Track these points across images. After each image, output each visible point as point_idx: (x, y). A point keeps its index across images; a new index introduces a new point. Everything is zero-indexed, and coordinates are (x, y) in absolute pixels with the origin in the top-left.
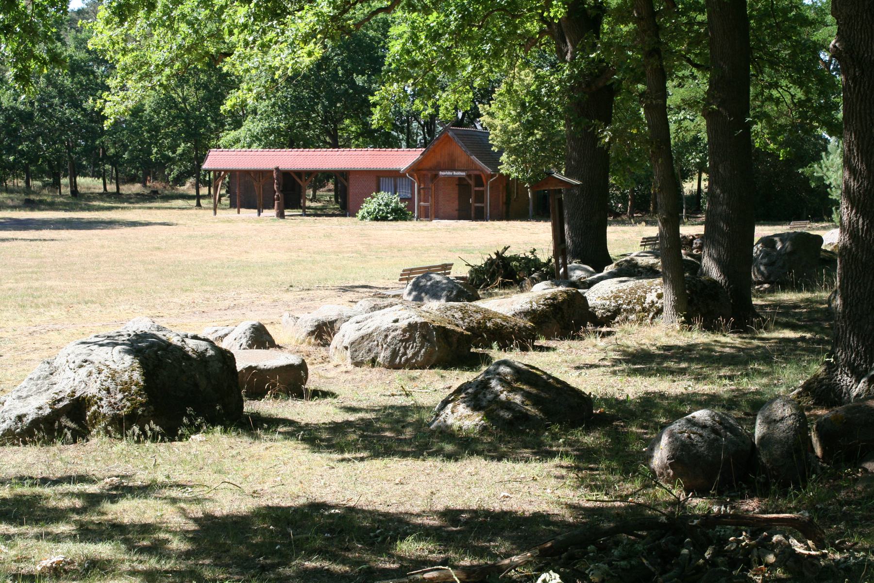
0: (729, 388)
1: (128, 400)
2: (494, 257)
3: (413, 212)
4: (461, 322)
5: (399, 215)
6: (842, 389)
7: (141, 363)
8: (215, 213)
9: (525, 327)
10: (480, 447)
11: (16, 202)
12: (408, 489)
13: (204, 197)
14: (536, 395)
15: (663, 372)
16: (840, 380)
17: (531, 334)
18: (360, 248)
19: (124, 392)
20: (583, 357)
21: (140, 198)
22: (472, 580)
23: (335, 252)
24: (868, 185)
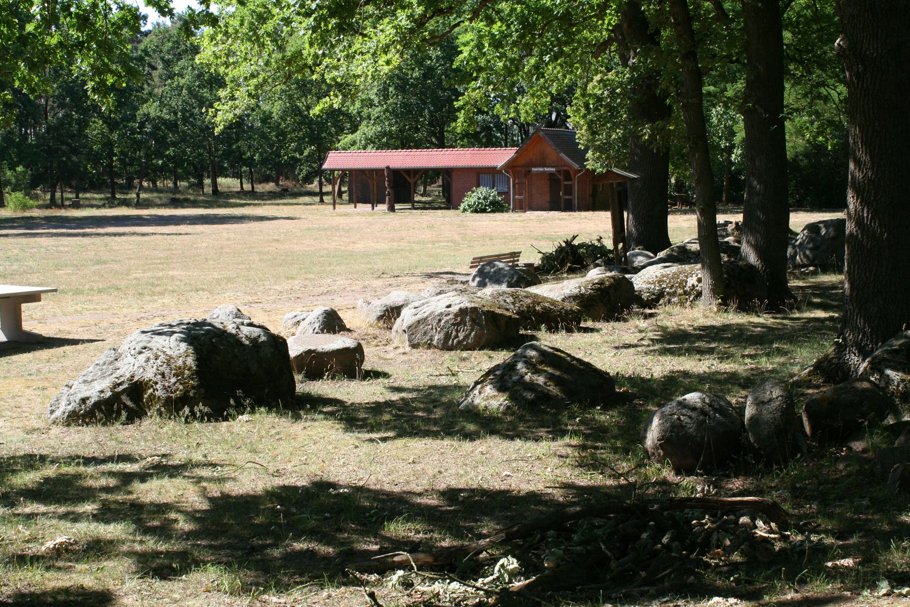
0: (749, 366)
1: (181, 384)
2: (564, 245)
3: (509, 205)
4: (512, 307)
5: (497, 207)
6: (850, 368)
7: (195, 349)
8: (334, 208)
9: (571, 310)
10: (498, 427)
11: (164, 201)
12: (419, 468)
13: (327, 194)
14: (558, 376)
15: (690, 351)
16: (848, 360)
17: (577, 317)
18: (456, 237)
19: (178, 376)
20: (624, 338)
21: (272, 196)
22: (439, 563)
23: (433, 243)
24: (872, 175)
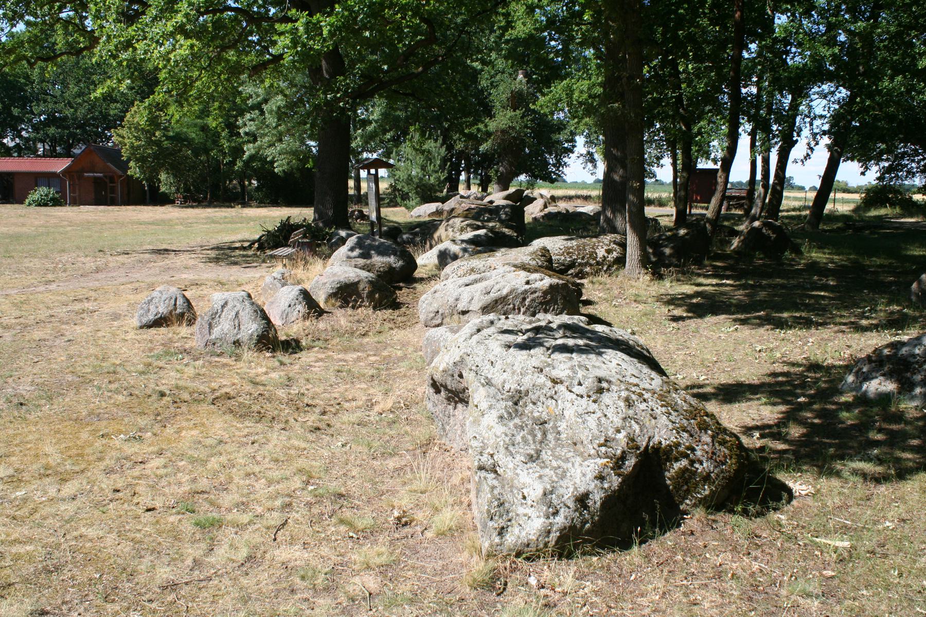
5: (56, 202)
